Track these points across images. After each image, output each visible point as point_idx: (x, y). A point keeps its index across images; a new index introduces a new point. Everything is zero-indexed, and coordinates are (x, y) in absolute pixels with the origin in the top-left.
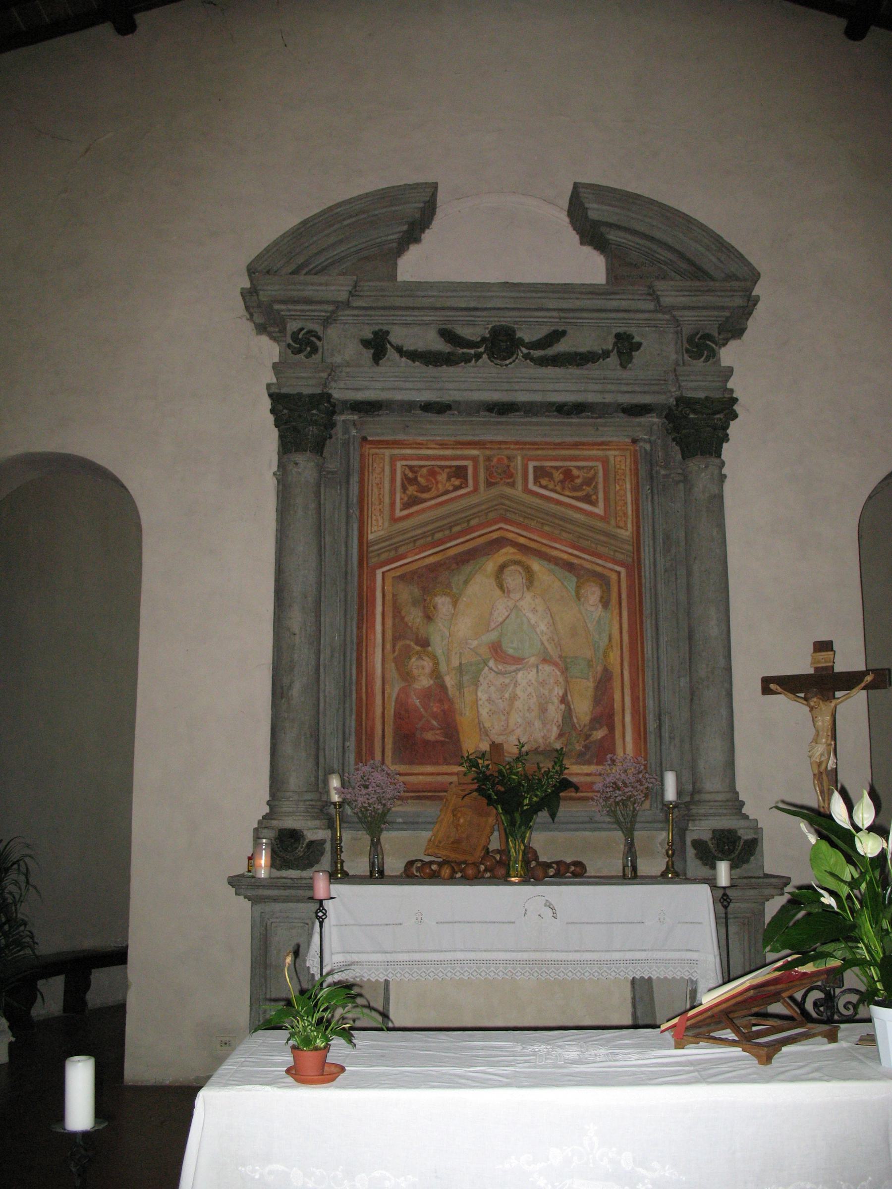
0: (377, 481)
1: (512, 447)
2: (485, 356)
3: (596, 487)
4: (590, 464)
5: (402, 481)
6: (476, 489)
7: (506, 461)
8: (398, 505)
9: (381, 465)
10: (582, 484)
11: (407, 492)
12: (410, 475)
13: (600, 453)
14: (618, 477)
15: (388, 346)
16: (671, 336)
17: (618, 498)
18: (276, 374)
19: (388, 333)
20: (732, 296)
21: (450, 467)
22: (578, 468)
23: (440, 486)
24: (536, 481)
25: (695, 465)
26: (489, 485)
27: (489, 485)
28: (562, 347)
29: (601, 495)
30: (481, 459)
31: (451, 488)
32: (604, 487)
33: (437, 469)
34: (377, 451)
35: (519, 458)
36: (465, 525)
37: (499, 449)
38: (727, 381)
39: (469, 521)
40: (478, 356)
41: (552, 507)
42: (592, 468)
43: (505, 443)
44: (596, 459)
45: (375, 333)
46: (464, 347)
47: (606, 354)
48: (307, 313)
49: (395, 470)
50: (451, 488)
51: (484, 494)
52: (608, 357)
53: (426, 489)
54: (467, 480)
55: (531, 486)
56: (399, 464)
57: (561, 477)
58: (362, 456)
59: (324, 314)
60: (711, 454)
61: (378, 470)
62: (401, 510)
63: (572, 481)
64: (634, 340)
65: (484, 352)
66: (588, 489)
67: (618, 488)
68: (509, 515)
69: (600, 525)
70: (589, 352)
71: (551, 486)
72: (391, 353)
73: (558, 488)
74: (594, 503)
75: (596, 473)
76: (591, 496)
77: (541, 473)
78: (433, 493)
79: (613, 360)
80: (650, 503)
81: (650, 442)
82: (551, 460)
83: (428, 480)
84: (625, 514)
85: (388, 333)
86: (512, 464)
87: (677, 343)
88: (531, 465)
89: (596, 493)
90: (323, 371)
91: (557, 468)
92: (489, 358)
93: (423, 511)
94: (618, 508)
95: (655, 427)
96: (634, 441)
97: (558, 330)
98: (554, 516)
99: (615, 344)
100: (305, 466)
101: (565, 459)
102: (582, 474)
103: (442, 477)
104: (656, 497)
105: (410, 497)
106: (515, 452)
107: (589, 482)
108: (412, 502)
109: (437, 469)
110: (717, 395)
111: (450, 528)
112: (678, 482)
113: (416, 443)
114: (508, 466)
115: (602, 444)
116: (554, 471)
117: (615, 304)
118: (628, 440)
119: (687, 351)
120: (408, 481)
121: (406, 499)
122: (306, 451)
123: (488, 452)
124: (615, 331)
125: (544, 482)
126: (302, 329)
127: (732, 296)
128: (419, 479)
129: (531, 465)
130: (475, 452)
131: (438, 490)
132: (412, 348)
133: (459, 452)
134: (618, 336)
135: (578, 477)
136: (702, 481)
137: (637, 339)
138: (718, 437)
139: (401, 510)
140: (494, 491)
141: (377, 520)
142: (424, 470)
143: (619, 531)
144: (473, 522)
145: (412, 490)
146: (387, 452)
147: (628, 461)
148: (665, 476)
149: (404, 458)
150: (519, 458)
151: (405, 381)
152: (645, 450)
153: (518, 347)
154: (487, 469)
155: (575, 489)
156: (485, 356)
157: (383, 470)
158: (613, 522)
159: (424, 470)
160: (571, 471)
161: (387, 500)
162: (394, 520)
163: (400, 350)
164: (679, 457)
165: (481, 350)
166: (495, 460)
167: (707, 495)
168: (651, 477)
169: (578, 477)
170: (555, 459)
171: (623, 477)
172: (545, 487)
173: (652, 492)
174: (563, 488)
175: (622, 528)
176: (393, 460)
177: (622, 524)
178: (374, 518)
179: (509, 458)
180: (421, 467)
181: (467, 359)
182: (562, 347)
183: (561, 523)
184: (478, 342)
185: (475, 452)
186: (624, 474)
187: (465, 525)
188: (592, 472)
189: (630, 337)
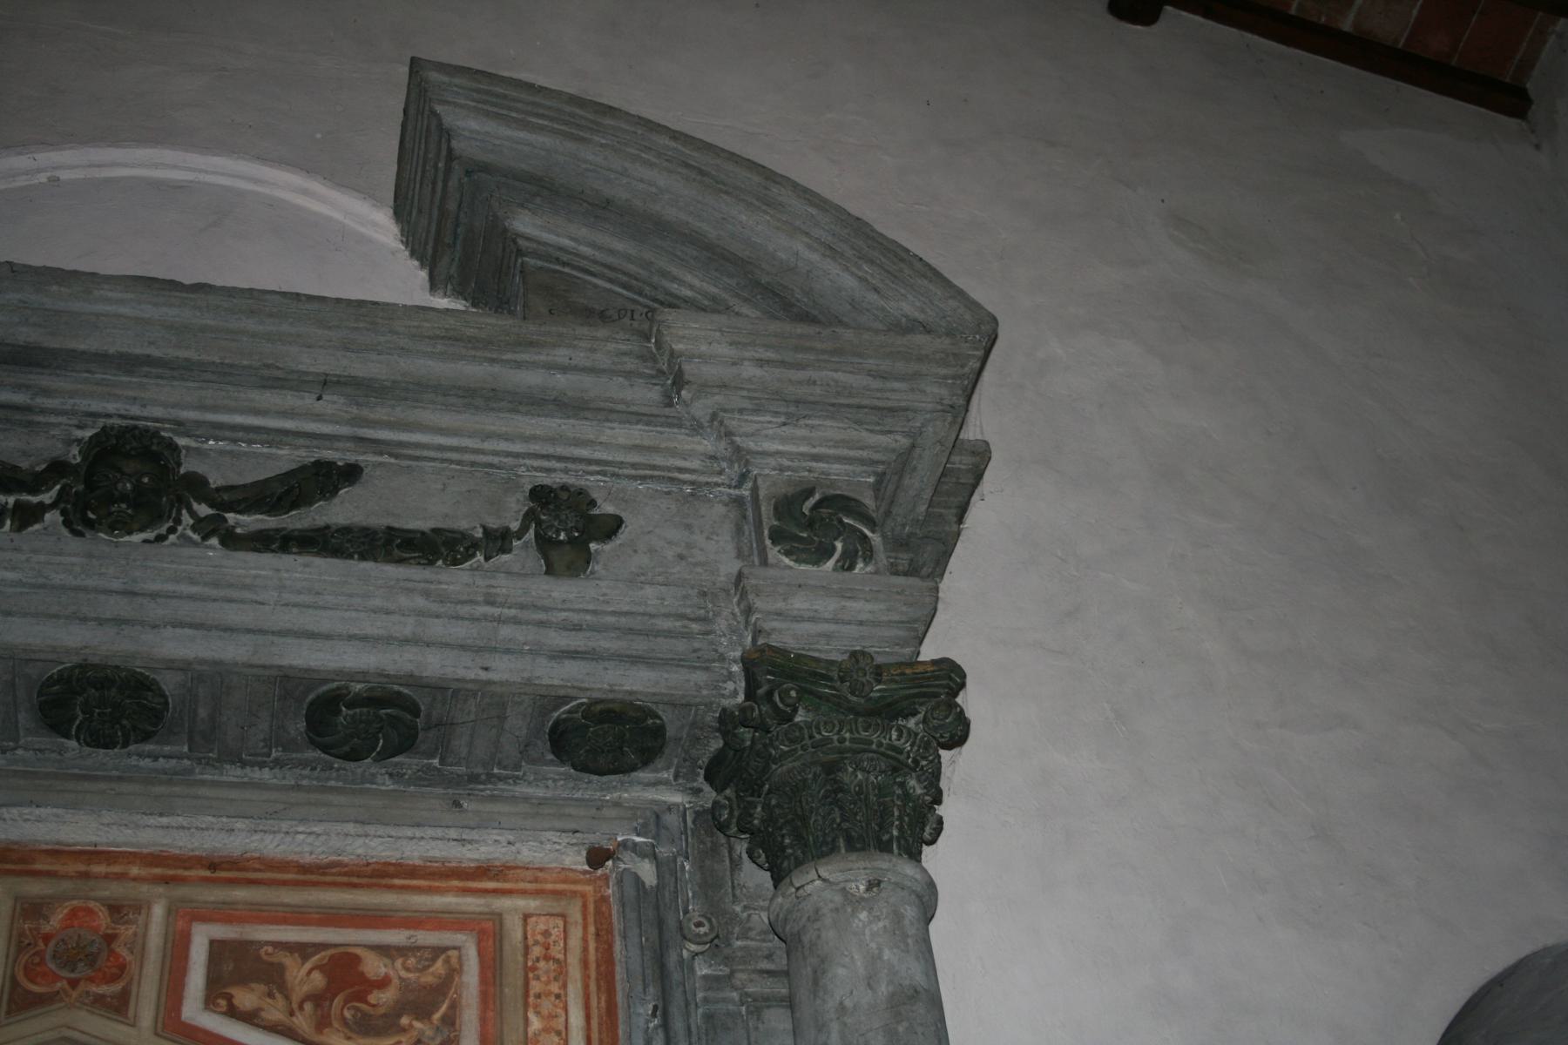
2: (53, 517)
3: (450, 1021)
7: (103, 920)
10: (400, 1009)
13: (471, 903)
14: (536, 987)
16: (720, 509)
22: (383, 950)
24: (216, 993)
25: (829, 881)
28: (340, 511)
35: (158, 911)
37: (86, 876)
42: (438, 951)
44: (458, 922)
47: (498, 540)
55: (193, 1010)
57: (318, 979)
60: (885, 848)
63: (361, 997)
64: (596, 511)
65: (53, 506)
67: (536, 1024)
70: (435, 531)
71: (275, 1013)
75: (454, 972)
77: (235, 968)
79: (522, 555)
81: (654, 857)
86: (126, 932)
87: (739, 531)
88: (200, 939)
91: (303, 950)
92: (67, 523)
95: (672, 820)
96: (597, 857)
99: (529, 516)
101: (332, 918)
102: (397, 970)
114: (110, 938)
115: (483, 871)
116: (289, 961)
119: (777, 536)
124: (532, 477)
125: (246, 998)
127: (917, 375)
129: (200, 939)
134: (541, 495)
135: (383, 983)
136: (856, 957)
138: (906, 796)
147: (576, 934)
148: (713, 982)
150: (158, 911)
152: (638, 881)
156: (53, 517)
160: (356, 959)
164: (765, 877)
165: (47, 498)
166: (55, 921)
167: (884, 989)
169: (383, 983)
170: (298, 917)
171: (555, 988)
179: (115, 909)
182: (340, 511)
184: (37, 475)
186: (561, 974)
188: (439, 967)
189: (579, 500)
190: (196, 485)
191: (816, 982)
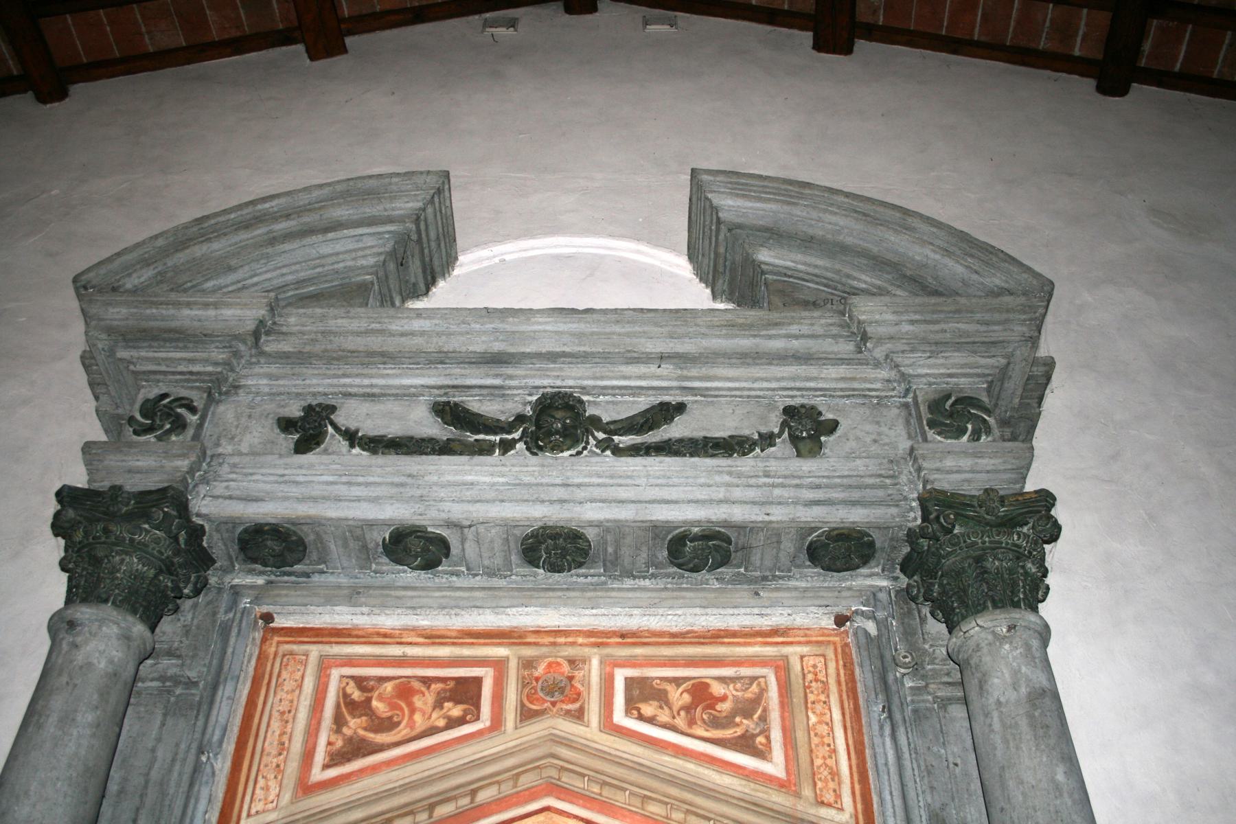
0: (284, 706)
1: (580, 640)
2: (520, 446)
3: (764, 719)
4: (746, 671)
5: (338, 706)
6: (497, 723)
7: (566, 668)
8: (320, 756)
9: (298, 675)
11: (345, 730)
12: (356, 695)
13: (769, 651)
14: (811, 697)
15: (330, 429)
16: (895, 411)
17: (815, 740)
18: (88, 464)
19: (333, 409)
20: (1007, 321)
21: (443, 680)
22: (722, 680)
23: (418, 717)
24: (631, 706)
25: (983, 628)
26: (526, 715)
27: (526, 715)
28: (676, 429)
29: (776, 735)
30: (513, 664)
31: (441, 723)
32: (783, 718)
33: (416, 685)
34: (295, 647)
35: (595, 662)
36: (465, 801)
37: (554, 644)
38: (1024, 479)
39: (474, 793)
40: (506, 446)
41: (668, 762)
42: (753, 679)
43: (566, 633)
45: (309, 409)
46: (479, 432)
47: (767, 440)
48: (181, 368)
49: (326, 686)
50: (441, 723)
51: (513, 734)
52: (772, 445)
53: (387, 725)
54: (477, 706)
55: (619, 717)
56: (335, 673)
57: (687, 698)
58: (262, 658)
59: (210, 369)
60: (1016, 605)
61: (288, 685)
62: (326, 767)
63: (712, 707)
64: (822, 418)
65: (520, 439)
66: (747, 724)
67: (813, 719)
68: (566, 779)
69: (778, 799)
70: (731, 437)
71: (664, 717)
72: (333, 439)
73: (680, 722)
74: (761, 754)
75: (763, 690)
76: (754, 736)
77: (640, 691)
78: (402, 731)
80: (888, 741)
82: (663, 665)
83: (393, 706)
84: (835, 774)
85: (333, 409)
86: (579, 674)
87: (908, 422)
88: (620, 676)
89: (766, 732)
90: (184, 456)
91: (677, 681)
92: (528, 449)
93: (375, 769)
94: (818, 762)
95: (882, 596)
96: (841, 620)
97: (668, 404)
98: (672, 781)
99: (784, 425)
100: (108, 638)
101: (692, 662)
102: (730, 690)
103: (425, 700)
104: (901, 732)
105: (349, 741)
106: (587, 650)
107: (747, 708)
108: (357, 749)
109: (416, 685)
110: (1004, 489)
111: (431, 808)
112: (944, 703)
113: (378, 634)
114: (571, 678)
115: (775, 632)
116: (669, 688)
117: (777, 345)
118: (828, 623)
120: (348, 705)
121: (339, 743)
122: (106, 601)
123: (528, 652)
124: (782, 402)
125: (648, 709)
126: (165, 396)
127: (1007, 321)
128: (375, 703)
129: (620, 676)
130: (501, 652)
131: (411, 724)
132: (373, 433)
133: (466, 652)
134: (789, 411)
135: (724, 699)
137: (829, 416)
138: (1026, 574)
139: (326, 767)
140: (537, 729)
141: (267, 789)
142: (389, 687)
143: (824, 812)
144: (482, 797)
145: (355, 725)
146: (315, 651)
149: (350, 661)
150: (595, 662)
151: (349, 483)
153: (588, 432)
154: (524, 683)
155: (716, 723)
156: (520, 446)
157: (300, 686)
158: (807, 792)
159: (389, 687)
160: (707, 686)
161: (297, 746)
162: (306, 788)
163: (352, 437)
165: (516, 435)
167: (1024, 690)
168: (881, 680)
169: (724, 699)
170: (672, 662)
171: (823, 697)
172: (651, 720)
173: (890, 717)
174: (692, 722)
175: (829, 805)
176: (324, 666)
177: (829, 797)
178: (261, 782)
179: (572, 662)
180: (382, 679)
181: (484, 449)
182: (676, 429)
183: (689, 796)
185: (501, 652)
186: (825, 689)
187: (465, 801)
188: (754, 688)
190: (596, 422)
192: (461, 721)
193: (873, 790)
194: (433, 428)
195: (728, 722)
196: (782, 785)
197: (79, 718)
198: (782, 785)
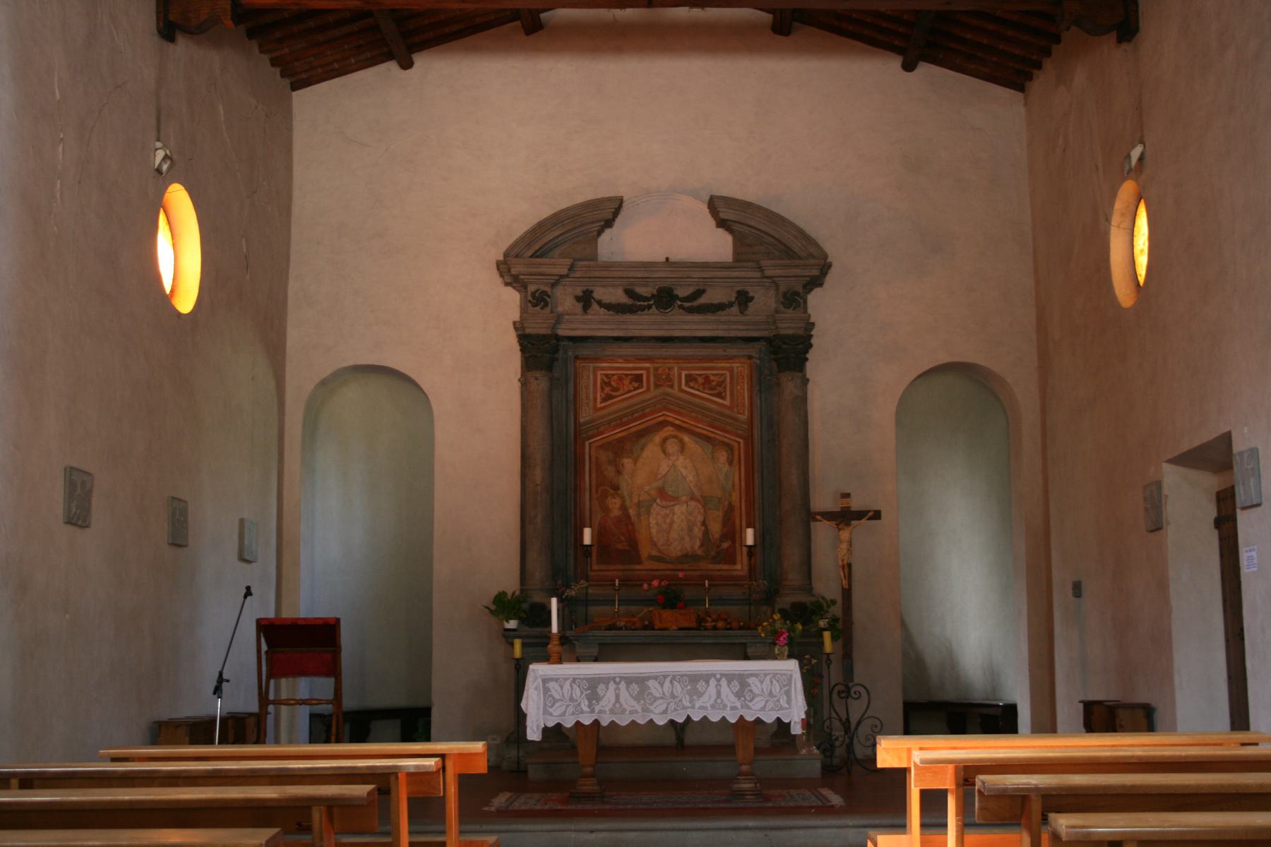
6: (648, 389)
8: (599, 400)
26: (657, 386)
27: (657, 386)
28: (703, 300)
40: (649, 307)
41: (697, 401)
47: (731, 305)
53: (616, 390)
56: (599, 373)
69: (727, 412)
72: (595, 306)
74: (724, 398)
77: (690, 379)
78: (621, 392)
79: (735, 309)
88: (684, 373)
101: (705, 369)
103: (626, 382)
107: (721, 384)
129: (684, 373)
140: (659, 391)
144: (647, 411)
145: (607, 389)
149: (603, 369)
155: (711, 389)
161: (591, 397)
170: (699, 369)
182: (703, 300)
185: (648, 365)
190: (677, 297)
191: (665, 299)
192: (636, 389)
193: (65, 799)
194: (624, 299)
195: (714, 389)
196: (729, 408)
197: (681, 458)
198: (729, 408)
